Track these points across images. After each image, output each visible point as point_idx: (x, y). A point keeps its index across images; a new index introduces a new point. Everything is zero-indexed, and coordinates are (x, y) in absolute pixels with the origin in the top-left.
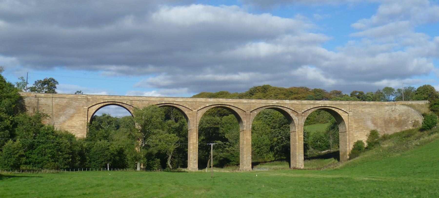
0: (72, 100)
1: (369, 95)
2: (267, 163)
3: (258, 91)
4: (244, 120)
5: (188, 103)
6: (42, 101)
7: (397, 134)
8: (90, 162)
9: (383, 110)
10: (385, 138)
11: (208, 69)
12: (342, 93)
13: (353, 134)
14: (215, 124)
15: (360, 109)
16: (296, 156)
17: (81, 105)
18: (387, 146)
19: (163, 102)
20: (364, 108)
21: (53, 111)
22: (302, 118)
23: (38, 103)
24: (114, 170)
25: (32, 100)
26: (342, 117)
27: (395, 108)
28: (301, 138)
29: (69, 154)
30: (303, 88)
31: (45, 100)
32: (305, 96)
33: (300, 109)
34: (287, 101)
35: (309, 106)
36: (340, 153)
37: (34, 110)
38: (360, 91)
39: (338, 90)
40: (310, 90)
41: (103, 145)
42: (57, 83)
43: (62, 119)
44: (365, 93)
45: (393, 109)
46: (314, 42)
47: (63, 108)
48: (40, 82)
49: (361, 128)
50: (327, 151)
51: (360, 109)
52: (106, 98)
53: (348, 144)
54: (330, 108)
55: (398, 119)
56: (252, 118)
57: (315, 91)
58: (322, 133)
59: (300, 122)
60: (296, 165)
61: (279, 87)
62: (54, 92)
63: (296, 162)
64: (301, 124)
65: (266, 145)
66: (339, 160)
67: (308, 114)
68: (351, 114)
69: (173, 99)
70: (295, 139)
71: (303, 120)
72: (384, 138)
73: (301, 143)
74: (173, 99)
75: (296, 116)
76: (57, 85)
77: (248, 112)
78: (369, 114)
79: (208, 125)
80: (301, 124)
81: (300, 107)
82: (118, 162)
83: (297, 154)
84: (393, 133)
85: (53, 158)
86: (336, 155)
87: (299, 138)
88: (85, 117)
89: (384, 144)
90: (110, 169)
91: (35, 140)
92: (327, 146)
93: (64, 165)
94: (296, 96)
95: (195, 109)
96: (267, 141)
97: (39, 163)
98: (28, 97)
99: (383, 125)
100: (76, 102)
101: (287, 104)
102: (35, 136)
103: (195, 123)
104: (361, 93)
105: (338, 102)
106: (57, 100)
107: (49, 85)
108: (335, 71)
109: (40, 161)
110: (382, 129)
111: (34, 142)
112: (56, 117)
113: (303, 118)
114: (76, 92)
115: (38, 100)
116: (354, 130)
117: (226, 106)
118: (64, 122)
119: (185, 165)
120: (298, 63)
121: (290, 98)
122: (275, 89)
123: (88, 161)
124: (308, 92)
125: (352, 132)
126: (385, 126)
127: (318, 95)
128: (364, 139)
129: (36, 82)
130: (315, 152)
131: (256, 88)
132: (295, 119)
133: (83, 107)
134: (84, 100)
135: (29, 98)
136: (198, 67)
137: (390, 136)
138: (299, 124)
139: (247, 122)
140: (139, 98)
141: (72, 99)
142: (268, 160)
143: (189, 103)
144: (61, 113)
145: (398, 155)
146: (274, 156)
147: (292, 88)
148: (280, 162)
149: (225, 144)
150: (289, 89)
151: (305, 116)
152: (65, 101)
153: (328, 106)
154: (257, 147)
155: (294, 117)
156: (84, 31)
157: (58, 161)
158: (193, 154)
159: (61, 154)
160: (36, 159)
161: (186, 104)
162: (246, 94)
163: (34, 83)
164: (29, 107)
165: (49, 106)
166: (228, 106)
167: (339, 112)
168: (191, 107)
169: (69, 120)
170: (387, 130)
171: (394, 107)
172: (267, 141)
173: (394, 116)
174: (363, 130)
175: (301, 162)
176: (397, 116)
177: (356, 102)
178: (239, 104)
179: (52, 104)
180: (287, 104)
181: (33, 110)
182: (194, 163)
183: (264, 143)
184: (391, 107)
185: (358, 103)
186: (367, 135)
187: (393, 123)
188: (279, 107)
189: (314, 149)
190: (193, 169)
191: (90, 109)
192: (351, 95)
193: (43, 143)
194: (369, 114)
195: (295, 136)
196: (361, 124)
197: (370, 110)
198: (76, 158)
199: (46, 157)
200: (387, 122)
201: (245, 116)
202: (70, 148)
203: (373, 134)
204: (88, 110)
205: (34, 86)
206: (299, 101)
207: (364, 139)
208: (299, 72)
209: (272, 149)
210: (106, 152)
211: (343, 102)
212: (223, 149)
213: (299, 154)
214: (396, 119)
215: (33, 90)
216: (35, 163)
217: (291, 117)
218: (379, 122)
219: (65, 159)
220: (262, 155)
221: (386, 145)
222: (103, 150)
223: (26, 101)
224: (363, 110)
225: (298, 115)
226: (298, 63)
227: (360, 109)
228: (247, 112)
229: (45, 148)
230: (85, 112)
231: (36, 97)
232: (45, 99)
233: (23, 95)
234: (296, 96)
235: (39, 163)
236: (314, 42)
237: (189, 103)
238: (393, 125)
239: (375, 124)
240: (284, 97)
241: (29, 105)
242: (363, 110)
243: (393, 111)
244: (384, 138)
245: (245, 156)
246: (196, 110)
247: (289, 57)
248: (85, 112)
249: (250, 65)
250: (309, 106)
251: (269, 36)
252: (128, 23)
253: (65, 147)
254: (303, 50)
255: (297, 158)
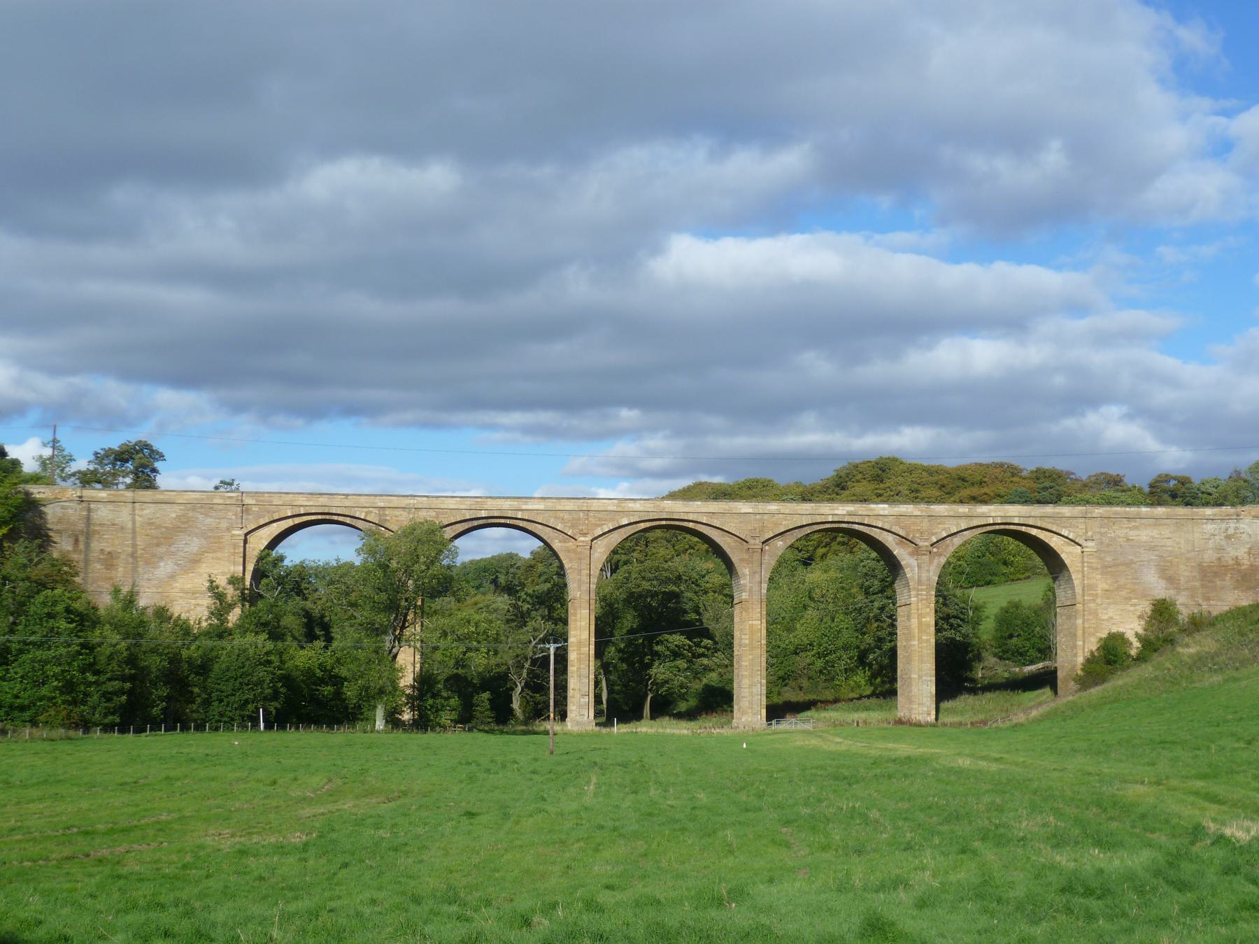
0: (194, 510)
1: (1208, 488)
2: (839, 705)
3: (860, 476)
4: (744, 570)
5: (561, 515)
6: (102, 513)
7: (1239, 614)
8: (207, 703)
9: (1197, 535)
10: (1197, 624)
11: (809, 418)
12: (1125, 480)
13: (1095, 613)
14: (668, 581)
15: (1120, 531)
16: (910, 684)
17: (224, 525)
18: (1192, 650)
19: (484, 514)
20: (1136, 528)
21: (134, 545)
22: (931, 562)
23: (88, 518)
24: (282, 727)
25: (70, 511)
26: (1063, 556)
27: (1236, 528)
28: (928, 625)
29: (124, 679)
30: (1002, 465)
31: (115, 509)
32: (1002, 491)
33: (925, 537)
34: (883, 508)
35: (955, 521)
36: (1060, 674)
37: (77, 541)
38: (1179, 474)
39: (1113, 472)
40: (1024, 474)
41: (251, 651)
42: (161, 457)
43: (165, 568)
44: (1196, 481)
45: (1231, 531)
46: (1132, 336)
47: (167, 536)
48: (109, 452)
49: (1124, 593)
50: (1040, 665)
51: (1121, 533)
52: (301, 501)
53: (1080, 643)
54: (1023, 529)
55: (1246, 562)
56: (770, 561)
57: (1040, 475)
58: (1030, 608)
59: (924, 575)
60: (910, 710)
61: (925, 463)
62: (151, 486)
63: (910, 701)
64: (929, 579)
65: (846, 648)
66: (1056, 693)
67: (952, 549)
68: (1091, 546)
69: (515, 504)
70: (908, 628)
71: (932, 568)
72: (1195, 625)
73: (928, 641)
74: (515, 504)
75: (912, 554)
76: (157, 465)
77: (756, 544)
78: (1152, 548)
79: (646, 585)
80: (929, 579)
81: (925, 524)
82: (312, 703)
83: (914, 676)
84: (1227, 608)
85: (69, 693)
86: (1047, 679)
87: (920, 623)
88: (235, 563)
89: (1187, 646)
90: (269, 726)
91: (14, 638)
92: (1040, 651)
93: (106, 716)
94: (975, 491)
95: (585, 535)
96: (847, 636)
97: (22, 708)
98: (56, 500)
99: (1197, 584)
100: (207, 515)
101: (880, 516)
102: (14, 623)
103: (586, 579)
104: (1184, 481)
105: (1049, 509)
106: (149, 511)
107: (136, 464)
108: (1197, 423)
109: (26, 702)
110: (1193, 597)
111: (9, 641)
112: (147, 563)
113: (936, 561)
114: (216, 482)
115: (89, 510)
116: (1099, 601)
117: (685, 524)
118: (172, 577)
119: (889, 693)
120: (1083, 397)
121: (957, 497)
122: (912, 469)
123: (199, 700)
124: (1015, 479)
125: (1092, 605)
126: (1203, 586)
127: (1045, 489)
128: (1131, 626)
129: (96, 454)
130: (1000, 670)
131: (856, 466)
132: (909, 565)
133: (228, 529)
134: (234, 508)
135: (60, 505)
136: (776, 411)
137: (1216, 618)
138: (920, 582)
139: (753, 573)
140: (405, 502)
141: (193, 506)
142: (852, 695)
143: (566, 516)
144: (162, 549)
145: (1217, 678)
146: (870, 681)
147: (965, 468)
148: (882, 700)
149: (698, 645)
150: (958, 469)
151: (940, 555)
152: (172, 513)
153: (1016, 521)
154: (819, 655)
155: (907, 557)
156: (442, 308)
157: (84, 702)
158: (580, 676)
159: (92, 678)
160: (17, 697)
161: (556, 518)
162: (824, 486)
163: (92, 458)
164: (59, 532)
165: (122, 528)
166: (691, 525)
167: (1054, 542)
168: (572, 527)
169: (186, 572)
170: (1208, 599)
171: (1232, 525)
172: (847, 636)
173: (1233, 553)
174: (1130, 599)
175: (925, 700)
176: (1241, 552)
177: (1107, 509)
178: (731, 520)
179: (134, 522)
180: (880, 516)
181: (72, 541)
182: (580, 706)
183: (840, 643)
184: (1224, 526)
185: (1116, 513)
186: (1140, 617)
187: (1228, 578)
188: (856, 527)
189: (1001, 658)
190: (578, 723)
191: (251, 538)
192: (1151, 486)
193: (38, 645)
194: (1152, 548)
195: (909, 617)
196: (1122, 581)
197: (1155, 533)
198: (155, 687)
199: (44, 691)
200: (1210, 574)
201: (745, 556)
202: (132, 660)
203: (1162, 611)
204: (245, 542)
205: (91, 467)
206: (923, 506)
207: (1131, 626)
208: (1092, 419)
209: (862, 660)
210: (261, 673)
211: (1066, 510)
212: (690, 661)
213: (920, 677)
214: (1238, 564)
215: (87, 479)
216: (11, 707)
217: (894, 557)
218: (1185, 572)
219: (108, 696)
220: (833, 679)
221: (1189, 649)
222: (291, 663)
223: (51, 513)
224: (1132, 534)
225: (917, 550)
226: (1083, 397)
227: (1121, 533)
228: (752, 541)
229: (46, 662)
230: (235, 546)
231: (81, 500)
232: (110, 507)
233: (41, 496)
234: (975, 491)
235: (22, 708)
236: (1132, 336)
237: (566, 516)
238: (1228, 581)
239: (1171, 580)
240: (938, 494)
241: (59, 527)
242: (1132, 534)
243: (1228, 537)
244: (1195, 625)
245: (746, 682)
246: (589, 538)
247: (1059, 380)
248: (235, 546)
249: (927, 404)
250: (955, 521)
251: (1010, 321)
252: (578, 287)
253: (111, 657)
254: (1100, 359)
255: (915, 690)
